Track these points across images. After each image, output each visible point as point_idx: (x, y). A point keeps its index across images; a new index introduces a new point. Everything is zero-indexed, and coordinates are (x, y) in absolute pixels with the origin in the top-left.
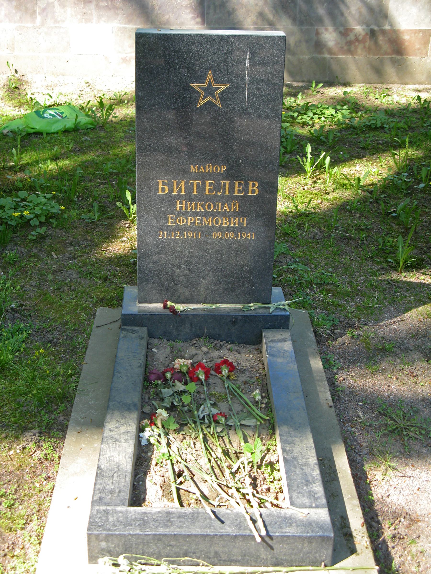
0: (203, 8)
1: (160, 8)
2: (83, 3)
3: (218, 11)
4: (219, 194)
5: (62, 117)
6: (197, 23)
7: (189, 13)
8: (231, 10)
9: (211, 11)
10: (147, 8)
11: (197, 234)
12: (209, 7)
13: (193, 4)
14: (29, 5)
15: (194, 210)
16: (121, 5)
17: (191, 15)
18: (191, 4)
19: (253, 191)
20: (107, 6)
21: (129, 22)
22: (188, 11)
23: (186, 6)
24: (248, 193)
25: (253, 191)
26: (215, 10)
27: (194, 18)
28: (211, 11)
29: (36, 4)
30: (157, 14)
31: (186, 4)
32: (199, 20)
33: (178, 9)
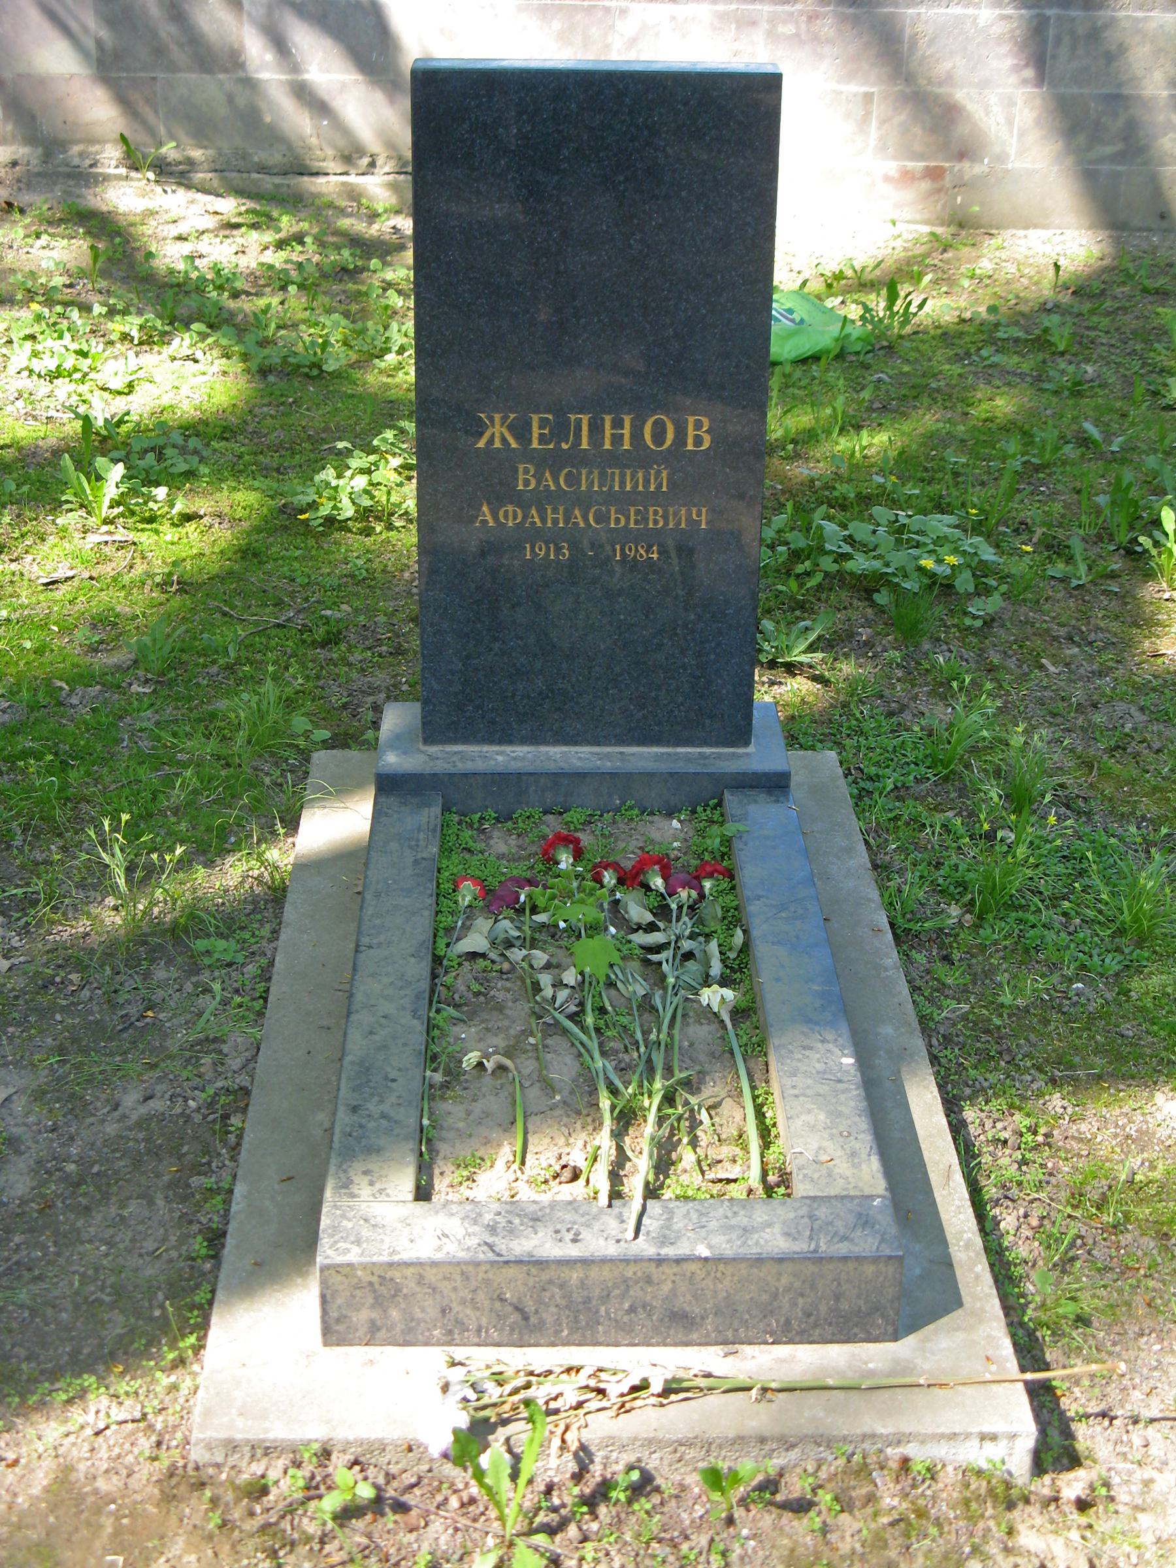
0: (1043, 42)
1: (932, 41)
2: (733, 26)
3: (1080, 51)
4: (565, 446)
5: (792, 321)
6: (1025, 82)
7: (1006, 56)
8: (1114, 47)
9: (1064, 51)
10: (901, 42)
11: (558, 550)
12: (1058, 40)
13: (1018, 32)
14: (593, 30)
15: (641, 488)
16: (832, 33)
17: (1010, 62)
18: (1012, 31)
19: (698, 441)
20: (797, 35)
21: (850, 76)
22: (1005, 49)
23: (999, 38)
24: (530, 442)
25: (698, 441)
26: (1073, 48)
27: (1016, 69)
28: (1064, 51)
29: (612, 27)
30: (924, 57)
31: (999, 31)
32: (1029, 73)
33: (979, 45)
